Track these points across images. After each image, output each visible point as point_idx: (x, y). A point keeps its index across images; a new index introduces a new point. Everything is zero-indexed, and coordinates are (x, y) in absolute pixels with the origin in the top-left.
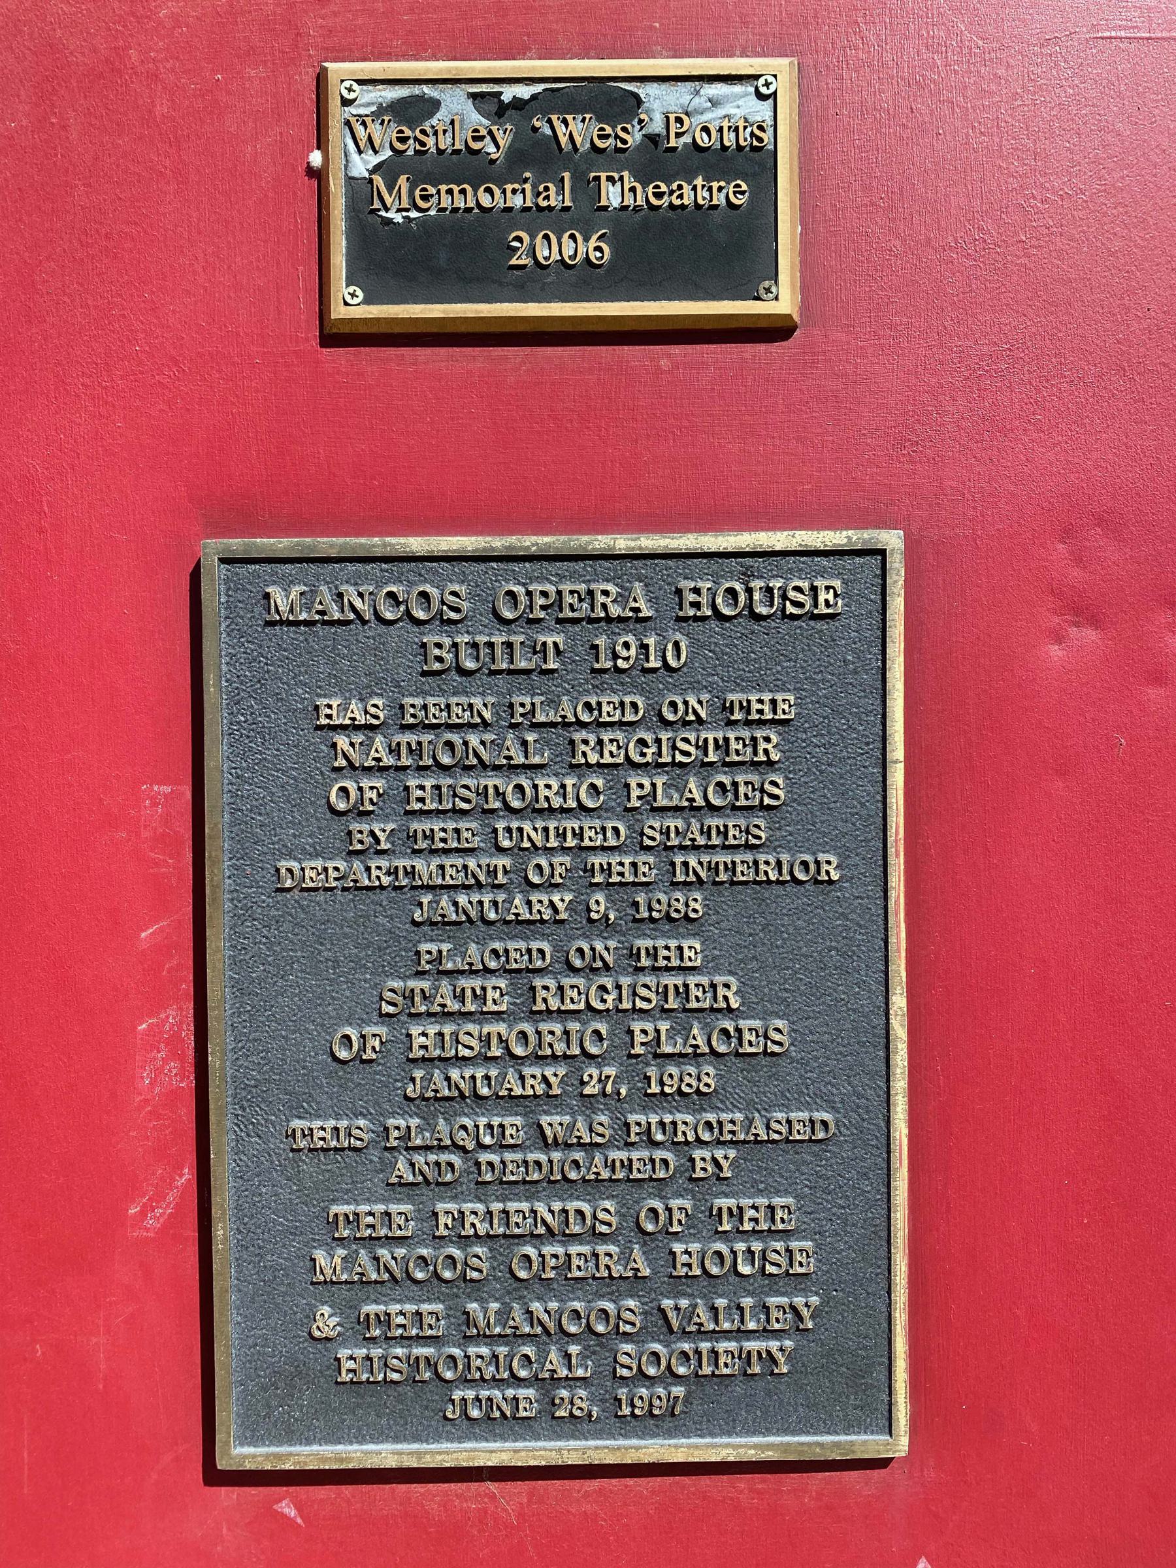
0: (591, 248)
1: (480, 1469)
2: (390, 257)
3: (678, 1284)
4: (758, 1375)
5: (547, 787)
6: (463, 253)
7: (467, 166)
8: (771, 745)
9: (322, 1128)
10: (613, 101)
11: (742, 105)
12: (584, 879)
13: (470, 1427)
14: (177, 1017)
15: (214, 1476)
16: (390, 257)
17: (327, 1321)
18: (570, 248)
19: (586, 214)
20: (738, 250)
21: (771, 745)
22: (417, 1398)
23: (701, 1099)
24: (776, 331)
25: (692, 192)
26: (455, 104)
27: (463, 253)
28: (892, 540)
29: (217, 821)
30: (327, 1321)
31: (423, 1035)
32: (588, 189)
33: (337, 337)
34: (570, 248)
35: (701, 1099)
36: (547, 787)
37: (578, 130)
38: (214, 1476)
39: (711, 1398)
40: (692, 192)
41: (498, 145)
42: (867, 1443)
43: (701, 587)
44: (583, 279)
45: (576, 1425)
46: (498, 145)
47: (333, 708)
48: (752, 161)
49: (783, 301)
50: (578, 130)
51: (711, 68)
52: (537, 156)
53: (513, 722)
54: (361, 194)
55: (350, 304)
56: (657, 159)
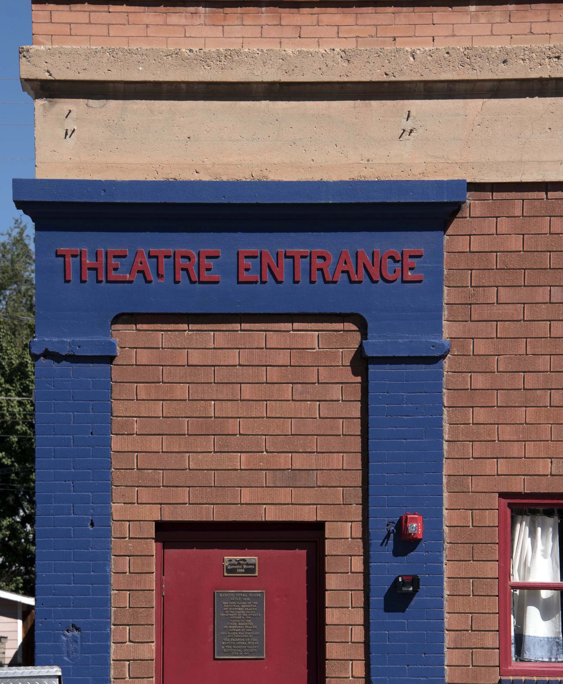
0: (243, 571)
1: (542, 94)
2: (229, 571)
3: (248, 645)
4: (254, 652)
5: (239, 609)
6: (233, 571)
7: (234, 565)
8: (255, 606)
9: (223, 633)
10: (244, 560)
11: (254, 561)
12: (242, 616)
13: (235, 655)
14: (212, 626)
15: (215, 659)
16: (229, 571)
17: (223, 647)
18: (241, 570)
19: (243, 568)
20: (253, 571)
21: (255, 606)
22: (229, 653)
23: (250, 632)
24: (256, 576)
25: (250, 567)
26: (233, 560)
27: (233, 571)
28: (264, 591)
29: (216, 611)
30: (223, 647)
31: (230, 627)
32: (243, 566)
33: (224, 576)
34: (241, 570)
35: (250, 632)
36: (239, 609)
37: (242, 562)
38: (215, 659)
39: (251, 653)
40: (250, 567)
41: (236, 563)
42: (262, 657)
43: (250, 595)
44: (243, 573)
45: (241, 655)
46: (236, 563)
47: (224, 603)
48: (255, 565)
49: (257, 574)
50: (242, 562)
51: (205, 60)
52: (239, 564)
53: (237, 604)
54: (227, 566)
55: (226, 574)
56: (247, 564)
